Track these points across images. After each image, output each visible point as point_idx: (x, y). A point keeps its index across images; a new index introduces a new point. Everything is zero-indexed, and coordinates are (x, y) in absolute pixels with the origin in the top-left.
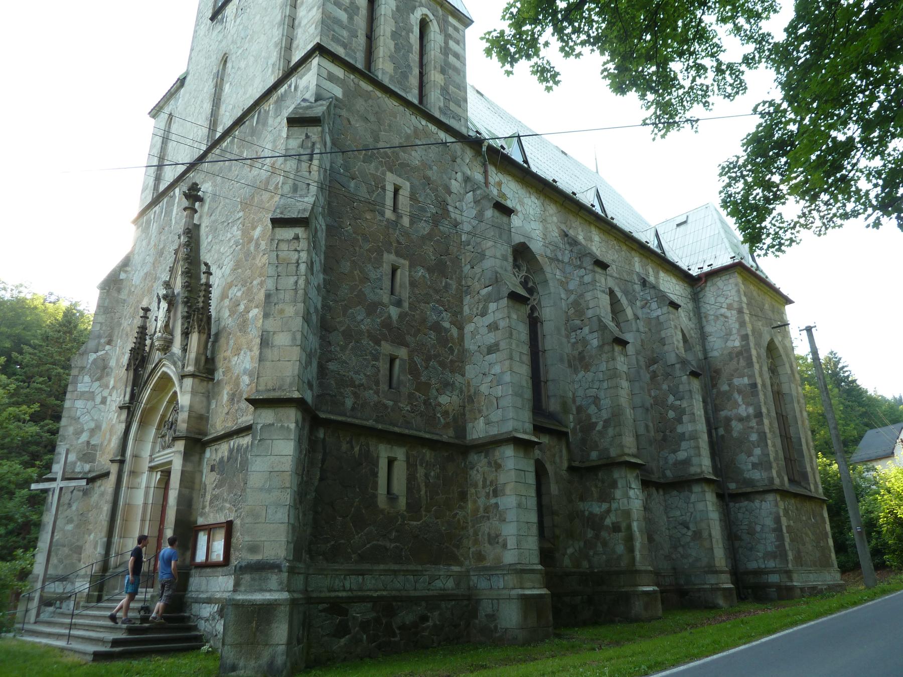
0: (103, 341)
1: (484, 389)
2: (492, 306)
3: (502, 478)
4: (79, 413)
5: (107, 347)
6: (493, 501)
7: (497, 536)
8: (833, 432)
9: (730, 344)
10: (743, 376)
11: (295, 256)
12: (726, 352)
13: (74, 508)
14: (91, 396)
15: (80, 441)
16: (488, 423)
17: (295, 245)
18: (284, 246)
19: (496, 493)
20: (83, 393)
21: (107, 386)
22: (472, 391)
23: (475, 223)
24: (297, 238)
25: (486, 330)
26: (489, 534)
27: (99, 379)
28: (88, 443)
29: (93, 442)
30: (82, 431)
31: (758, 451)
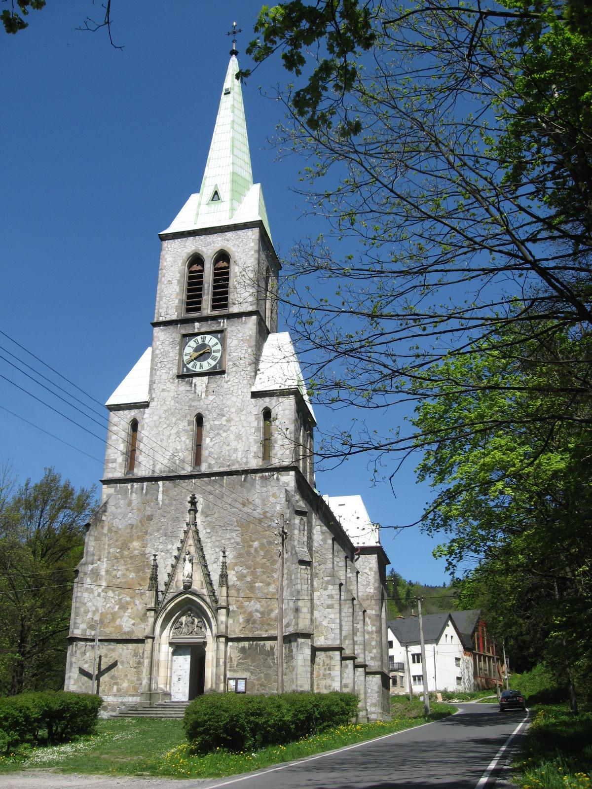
0: (96, 558)
1: (325, 623)
3: (333, 663)
5: (99, 562)
6: (328, 672)
7: (330, 686)
8: (359, 626)
9: (368, 590)
10: (372, 610)
11: (306, 576)
12: (365, 594)
14: (91, 591)
16: (326, 639)
17: (306, 572)
18: (302, 571)
19: (330, 669)
22: (318, 623)
23: (321, 543)
25: (326, 597)
26: (325, 686)
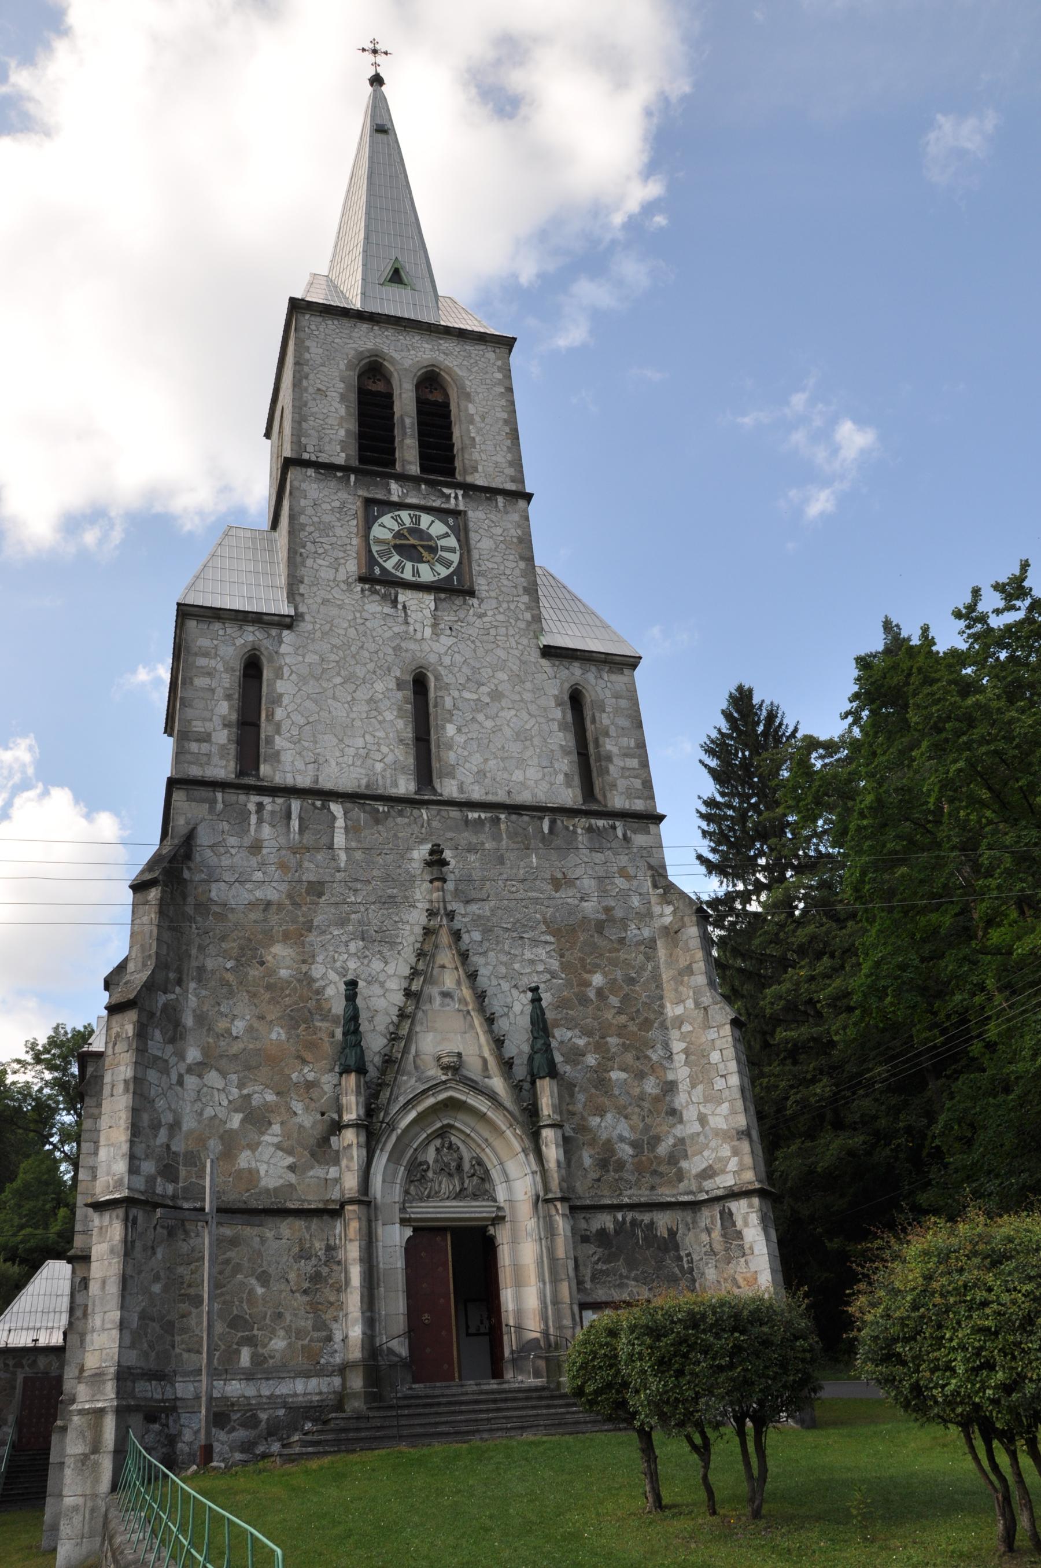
4: (153, 1092)
13: (159, 1256)
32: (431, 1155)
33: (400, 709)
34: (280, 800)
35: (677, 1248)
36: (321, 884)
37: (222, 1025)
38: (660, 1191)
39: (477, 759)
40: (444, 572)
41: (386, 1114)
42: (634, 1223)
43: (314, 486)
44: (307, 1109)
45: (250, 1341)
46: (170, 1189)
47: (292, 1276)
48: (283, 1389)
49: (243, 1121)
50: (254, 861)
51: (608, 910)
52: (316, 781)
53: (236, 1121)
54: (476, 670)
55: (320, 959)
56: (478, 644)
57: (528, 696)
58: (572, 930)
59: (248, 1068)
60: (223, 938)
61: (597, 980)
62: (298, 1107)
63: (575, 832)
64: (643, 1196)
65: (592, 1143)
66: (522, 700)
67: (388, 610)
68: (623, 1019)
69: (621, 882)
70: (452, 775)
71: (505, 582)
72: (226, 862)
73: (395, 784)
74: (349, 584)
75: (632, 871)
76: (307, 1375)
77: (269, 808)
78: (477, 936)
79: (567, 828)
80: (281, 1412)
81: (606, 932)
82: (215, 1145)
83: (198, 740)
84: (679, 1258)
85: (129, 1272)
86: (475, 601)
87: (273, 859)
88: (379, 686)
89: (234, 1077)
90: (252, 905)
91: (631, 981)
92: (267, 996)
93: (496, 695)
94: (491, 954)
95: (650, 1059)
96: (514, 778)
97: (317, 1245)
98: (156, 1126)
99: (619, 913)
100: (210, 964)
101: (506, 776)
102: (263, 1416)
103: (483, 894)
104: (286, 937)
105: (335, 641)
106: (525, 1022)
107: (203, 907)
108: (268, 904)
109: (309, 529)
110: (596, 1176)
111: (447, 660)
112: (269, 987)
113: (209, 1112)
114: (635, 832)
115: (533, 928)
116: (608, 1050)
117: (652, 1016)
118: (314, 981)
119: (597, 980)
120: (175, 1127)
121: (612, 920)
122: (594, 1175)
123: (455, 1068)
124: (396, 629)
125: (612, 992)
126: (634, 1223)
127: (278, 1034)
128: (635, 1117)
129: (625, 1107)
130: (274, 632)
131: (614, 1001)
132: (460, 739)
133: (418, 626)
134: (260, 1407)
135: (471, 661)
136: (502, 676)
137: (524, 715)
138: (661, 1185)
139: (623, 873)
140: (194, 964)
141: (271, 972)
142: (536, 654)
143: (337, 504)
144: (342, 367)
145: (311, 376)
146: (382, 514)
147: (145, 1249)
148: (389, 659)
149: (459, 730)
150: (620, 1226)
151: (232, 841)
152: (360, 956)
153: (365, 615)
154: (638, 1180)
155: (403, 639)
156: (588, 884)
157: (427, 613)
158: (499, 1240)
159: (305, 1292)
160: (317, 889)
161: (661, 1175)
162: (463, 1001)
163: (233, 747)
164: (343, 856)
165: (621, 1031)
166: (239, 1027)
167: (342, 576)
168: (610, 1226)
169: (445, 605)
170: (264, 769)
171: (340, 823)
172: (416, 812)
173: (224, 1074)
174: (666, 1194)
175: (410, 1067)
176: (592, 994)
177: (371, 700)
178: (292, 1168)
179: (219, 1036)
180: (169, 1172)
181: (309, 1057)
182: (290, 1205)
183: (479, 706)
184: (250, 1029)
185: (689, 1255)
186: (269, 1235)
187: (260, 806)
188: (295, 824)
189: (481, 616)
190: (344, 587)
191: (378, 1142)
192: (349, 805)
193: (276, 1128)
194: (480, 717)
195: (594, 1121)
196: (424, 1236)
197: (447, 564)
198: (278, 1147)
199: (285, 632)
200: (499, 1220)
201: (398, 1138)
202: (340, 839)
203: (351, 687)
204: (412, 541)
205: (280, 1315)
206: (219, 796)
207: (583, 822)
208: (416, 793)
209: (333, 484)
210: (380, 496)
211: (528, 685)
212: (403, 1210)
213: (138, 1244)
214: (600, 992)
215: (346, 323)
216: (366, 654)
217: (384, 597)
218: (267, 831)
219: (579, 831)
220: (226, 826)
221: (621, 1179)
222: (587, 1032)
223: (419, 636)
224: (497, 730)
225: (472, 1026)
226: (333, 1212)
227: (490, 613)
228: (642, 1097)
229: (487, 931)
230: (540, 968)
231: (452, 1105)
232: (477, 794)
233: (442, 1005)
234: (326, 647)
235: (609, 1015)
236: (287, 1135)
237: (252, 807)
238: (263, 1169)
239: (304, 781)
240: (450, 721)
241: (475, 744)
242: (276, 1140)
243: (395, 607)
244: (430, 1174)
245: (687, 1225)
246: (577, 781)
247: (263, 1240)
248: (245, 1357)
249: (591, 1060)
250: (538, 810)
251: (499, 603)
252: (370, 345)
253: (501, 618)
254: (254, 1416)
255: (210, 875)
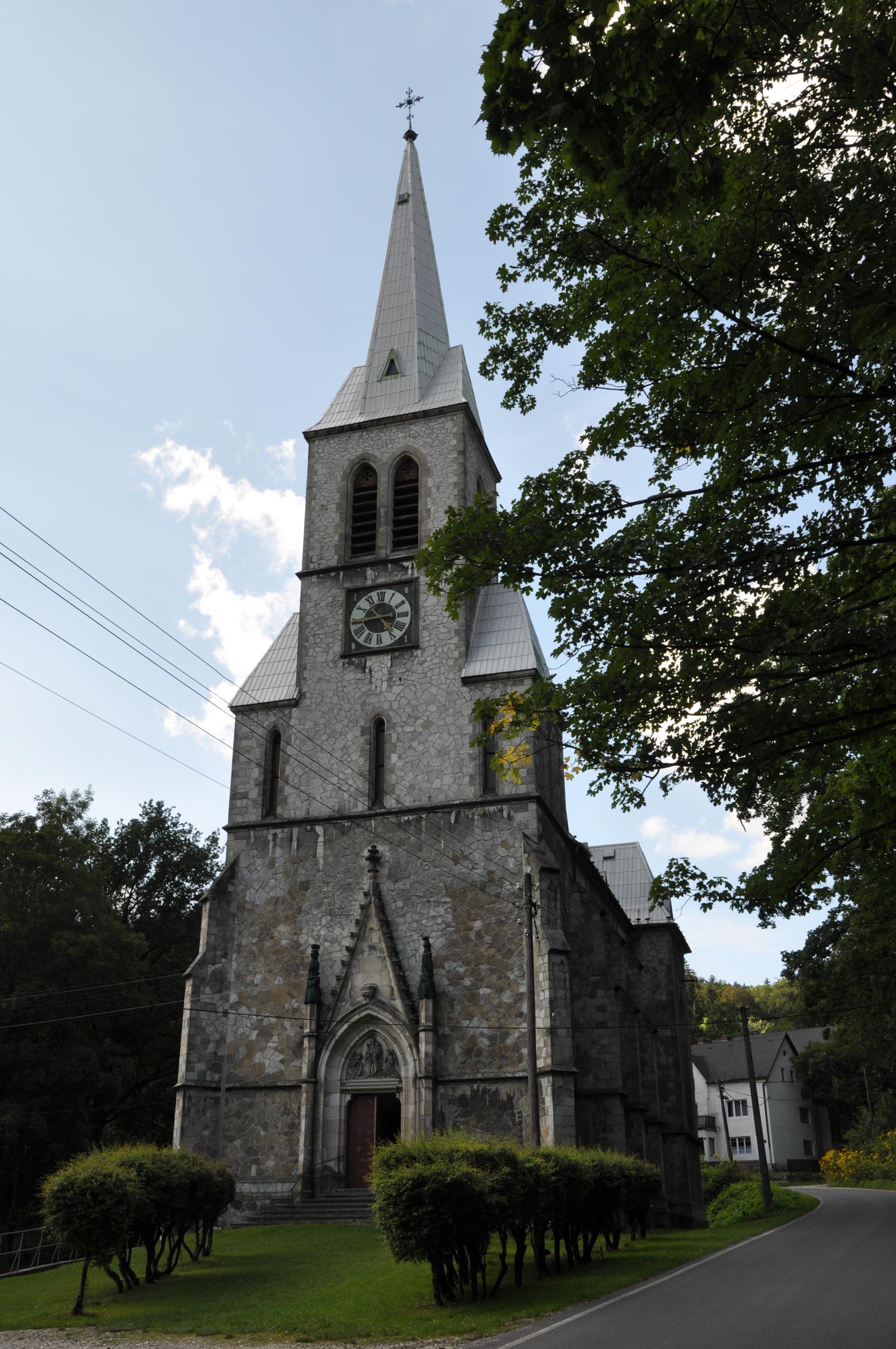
2: (600, 993)
4: (204, 1024)
13: (208, 1115)
15: (208, 1051)
20: (206, 1004)
21: (227, 1000)
24: (562, 963)
27: (219, 991)
28: (215, 1053)
29: (220, 1054)
30: (209, 1042)
31: (673, 1098)
32: (364, 1050)
33: (362, 750)
34: (286, 830)
35: (512, 1108)
36: (308, 882)
37: (249, 978)
38: (505, 1069)
39: (410, 776)
40: (398, 634)
41: (329, 1026)
42: (484, 1090)
43: (316, 589)
44: (292, 1026)
45: (256, 1162)
46: (217, 1077)
47: (279, 1125)
48: (271, 1189)
49: (258, 1035)
50: (270, 872)
51: (491, 873)
52: (308, 813)
53: (254, 1035)
54: (414, 708)
55: (304, 931)
56: (418, 686)
57: (449, 720)
58: (464, 891)
59: (262, 1003)
60: (252, 925)
61: (478, 925)
62: (287, 1024)
63: (473, 819)
64: (491, 1072)
65: (462, 1038)
66: (446, 724)
67: (359, 675)
68: (492, 951)
69: (501, 851)
70: (393, 792)
71: (442, 630)
72: (255, 876)
73: (356, 806)
74: (334, 662)
75: (510, 842)
76: (283, 1181)
77: (280, 836)
78: (400, 904)
79: (467, 817)
80: (268, 1202)
81: (487, 890)
82: (243, 1050)
83: (241, 799)
84: (514, 1115)
85: (186, 1125)
86: (419, 652)
87: (281, 869)
88: (350, 736)
89: (254, 1009)
90: (268, 902)
91: (501, 923)
92: (274, 958)
93: (427, 725)
94: (409, 915)
95: (508, 978)
96: (434, 786)
97: (294, 1106)
98: (206, 1043)
99: (499, 874)
100: (244, 942)
101: (428, 785)
102: (259, 1203)
103: (407, 874)
104: (287, 918)
105: (324, 708)
106: (419, 959)
107: (241, 908)
108: (278, 899)
109: (311, 626)
110: (462, 1060)
111: (395, 705)
112: (276, 952)
113: (241, 1031)
114: (516, 811)
115: (437, 894)
116: (480, 974)
117: (513, 947)
118: (301, 946)
119: (478, 925)
120: (221, 1040)
121: (491, 881)
122: (461, 1060)
123: (373, 993)
124: (363, 690)
125: (488, 932)
126: (484, 1090)
127: (279, 981)
128: (493, 1020)
129: (487, 1013)
130: (286, 712)
131: (488, 939)
132: (400, 764)
133: (378, 683)
134: (257, 1198)
135: (412, 702)
136: (433, 708)
137: (445, 736)
138: (506, 1065)
139: (504, 844)
140: (236, 942)
141: (277, 943)
142: (459, 683)
143: (330, 599)
144: (339, 479)
145: (318, 496)
146: (359, 599)
147: (198, 1111)
148: (358, 713)
149: (400, 757)
150: (475, 1094)
151: (259, 861)
152: (329, 926)
153: (345, 683)
154: (491, 1062)
155: (368, 696)
156: (477, 856)
157: (385, 671)
158: (402, 1101)
159: (286, 1134)
160: (305, 886)
161: (507, 1058)
162: (381, 950)
163: (260, 799)
164: (322, 862)
165: (490, 960)
166: (258, 978)
167: (330, 658)
168: (468, 1093)
169: (398, 661)
170: (279, 810)
171: (321, 839)
172: (368, 823)
173: (249, 1008)
174: (509, 1072)
175: (347, 996)
176: (472, 936)
177: (345, 747)
178: (282, 1061)
179: (247, 985)
180: (215, 1065)
181: (295, 993)
182: (279, 1084)
183: (415, 735)
184: (264, 980)
185: (520, 1112)
186: (269, 1101)
187: (275, 835)
188: (295, 844)
189: (421, 664)
190: (331, 665)
191: (323, 1044)
192: (327, 826)
193: (275, 1038)
194: (415, 744)
195: (466, 1023)
196: (358, 1098)
197: (400, 626)
198: (276, 1049)
199: (294, 710)
200: (399, 1090)
201: (337, 1041)
202: (320, 850)
203: (331, 741)
204: (378, 616)
205: (272, 1147)
206: (252, 833)
207: (480, 810)
208: (369, 809)
209: (328, 584)
210: (359, 584)
211: (451, 711)
212: (342, 1084)
213: (193, 1110)
214: (479, 934)
215: (343, 437)
216: (343, 713)
217: (357, 666)
218: (278, 851)
219: (476, 817)
220: (255, 852)
221: (479, 1061)
222: (467, 963)
223: (378, 690)
224: (426, 751)
225: (386, 967)
226: (297, 1088)
227: (429, 659)
228: (499, 1006)
229: (407, 900)
230: (439, 921)
231: (370, 1019)
232: (408, 802)
233: (369, 955)
234: (318, 714)
235: (483, 949)
236: (281, 1042)
237: (270, 837)
238: (267, 1062)
239: (300, 814)
240: (394, 752)
241: (409, 765)
242: (274, 1045)
243: (364, 672)
244: (363, 1061)
245: (521, 1092)
246: (478, 779)
247: (266, 1104)
248: (253, 1171)
249: (467, 982)
250: (448, 807)
251: (436, 649)
252: (360, 452)
253: (436, 661)
254: (254, 1203)
255: (246, 886)
